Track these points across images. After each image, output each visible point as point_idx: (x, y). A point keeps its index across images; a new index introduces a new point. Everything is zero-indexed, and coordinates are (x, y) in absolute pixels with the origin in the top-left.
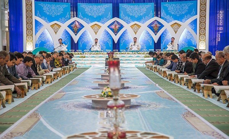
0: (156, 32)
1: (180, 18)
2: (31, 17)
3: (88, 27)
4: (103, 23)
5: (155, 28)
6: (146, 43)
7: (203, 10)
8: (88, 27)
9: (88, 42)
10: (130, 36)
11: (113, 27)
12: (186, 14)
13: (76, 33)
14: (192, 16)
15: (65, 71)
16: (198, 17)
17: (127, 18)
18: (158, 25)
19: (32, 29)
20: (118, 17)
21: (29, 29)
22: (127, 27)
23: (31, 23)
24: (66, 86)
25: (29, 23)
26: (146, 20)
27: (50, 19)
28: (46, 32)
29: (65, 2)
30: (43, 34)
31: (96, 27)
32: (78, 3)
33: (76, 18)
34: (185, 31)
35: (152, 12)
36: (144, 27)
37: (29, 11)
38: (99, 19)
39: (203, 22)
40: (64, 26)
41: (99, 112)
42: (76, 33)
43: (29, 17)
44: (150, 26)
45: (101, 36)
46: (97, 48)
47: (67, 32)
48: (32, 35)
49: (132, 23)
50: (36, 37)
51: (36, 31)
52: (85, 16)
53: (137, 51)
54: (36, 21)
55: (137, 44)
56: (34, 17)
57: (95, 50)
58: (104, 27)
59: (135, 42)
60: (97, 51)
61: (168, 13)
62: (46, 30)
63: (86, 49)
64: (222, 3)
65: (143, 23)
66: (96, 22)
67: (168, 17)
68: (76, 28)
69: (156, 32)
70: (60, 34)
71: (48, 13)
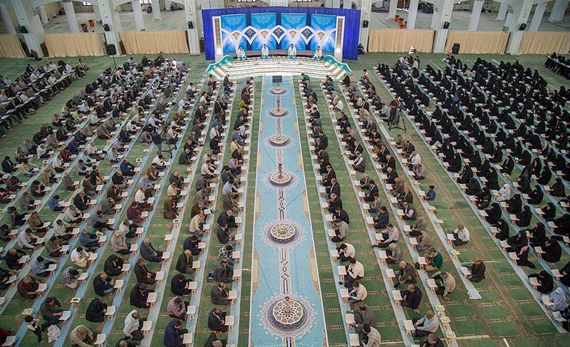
3: (258, 32)
5: (307, 34)
7: (340, 26)
8: (258, 32)
12: (329, 25)
13: (250, 37)
15: (53, 133)
16: (336, 29)
20: (251, 25)
21: (218, 39)
22: (287, 32)
25: (218, 35)
29: (167, 9)
30: (228, 39)
36: (299, 31)
37: (217, 26)
38: (294, 26)
39: (339, 35)
40: (242, 33)
42: (250, 37)
43: (218, 30)
47: (272, 36)
49: (262, 31)
50: (223, 44)
51: (223, 39)
56: (221, 29)
58: (270, 32)
61: (316, 23)
66: (264, 29)
67: (316, 26)
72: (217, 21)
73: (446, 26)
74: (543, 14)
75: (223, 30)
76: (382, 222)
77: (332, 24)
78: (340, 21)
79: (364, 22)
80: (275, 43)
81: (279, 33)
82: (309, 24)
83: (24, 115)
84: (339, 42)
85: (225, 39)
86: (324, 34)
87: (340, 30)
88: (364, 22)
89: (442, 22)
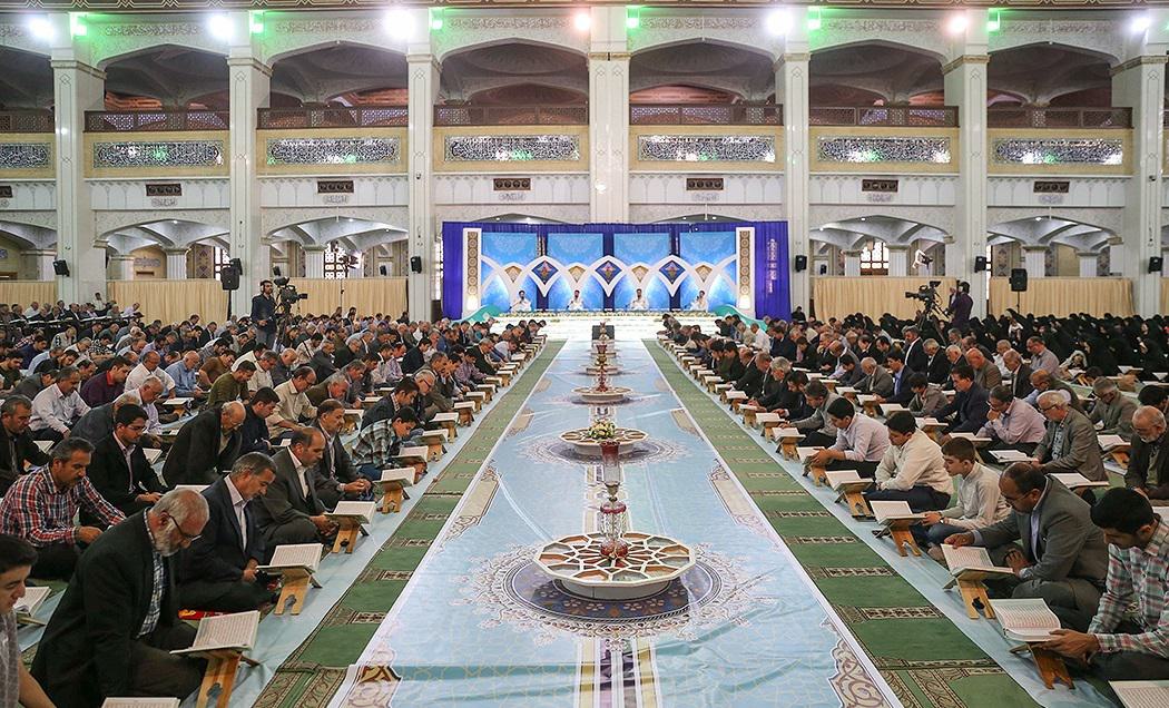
0: (672, 280)
1: (710, 257)
2: (476, 257)
4: (589, 264)
5: (672, 272)
6: (655, 295)
7: (745, 247)
9: (564, 295)
10: (631, 285)
11: (604, 269)
12: (720, 251)
13: (608, 280)
14: (730, 255)
17: (625, 256)
18: (676, 269)
19: (476, 276)
21: (474, 276)
22: (626, 270)
23: (476, 267)
24: (500, 439)
25: (473, 266)
26: (657, 261)
27: (504, 258)
28: (498, 279)
31: (577, 271)
32: (430, 445)
33: (544, 258)
34: (654, 278)
35: (667, 247)
37: (473, 248)
41: (587, 466)
42: (608, 280)
44: (662, 270)
45: (584, 285)
46: (578, 306)
48: (476, 285)
51: (483, 279)
52: (560, 255)
53: (643, 312)
54: (483, 262)
55: (642, 299)
56: (480, 257)
57: (575, 309)
58: (590, 270)
59: (639, 296)
60: (579, 311)
61: (691, 249)
62: (498, 277)
63: (1016, 472)
64: (773, 235)
65: (652, 264)
68: (545, 273)
69: (672, 280)
70: (521, 283)
71: (502, 250)
72: (473, 238)
73: (1155, 265)
74: (1081, 269)
75: (487, 260)
76: (750, 670)
77: (729, 248)
78: (744, 237)
79: (798, 257)
80: (601, 296)
81: (609, 273)
82: (674, 252)
83: (362, 348)
84: (744, 284)
85: (487, 282)
86: (646, 270)
87: (745, 257)
88: (798, 257)
89: (1142, 258)
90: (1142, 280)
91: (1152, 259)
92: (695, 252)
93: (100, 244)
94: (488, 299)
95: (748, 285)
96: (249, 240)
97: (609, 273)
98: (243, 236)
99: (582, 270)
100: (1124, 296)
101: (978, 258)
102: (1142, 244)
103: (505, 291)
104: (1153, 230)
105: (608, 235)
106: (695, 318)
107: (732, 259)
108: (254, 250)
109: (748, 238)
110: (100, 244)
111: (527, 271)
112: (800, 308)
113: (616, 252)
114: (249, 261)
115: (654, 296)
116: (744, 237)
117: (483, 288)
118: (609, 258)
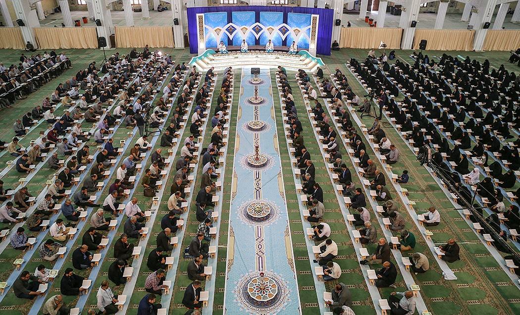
5: (284, 31)
7: (314, 24)
12: (304, 23)
22: (265, 29)
23: (203, 30)
25: (202, 30)
37: (201, 22)
56: (204, 26)
58: (250, 29)
72: (201, 18)
78: (315, 19)
80: (254, 38)
81: (257, 30)
82: (285, 21)
85: (208, 35)
87: (314, 27)
90: (479, 32)
91: (486, 23)
92: (293, 22)
93: (33, 8)
94: (208, 41)
95: (314, 39)
96: (101, 10)
97: (257, 30)
98: (99, 8)
99: (247, 29)
100: (470, 38)
101: (413, 22)
102: (485, 14)
103: (214, 37)
104: (491, 10)
105: (258, 11)
106: (292, 57)
107: (309, 27)
108: (104, 14)
109: (316, 20)
110: (33, 8)
111: (224, 30)
112: (336, 41)
113: (261, 20)
114: (103, 20)
115: (276, 39)
116: (315, 19)
117: (206, 38)
118: (257, 23)
